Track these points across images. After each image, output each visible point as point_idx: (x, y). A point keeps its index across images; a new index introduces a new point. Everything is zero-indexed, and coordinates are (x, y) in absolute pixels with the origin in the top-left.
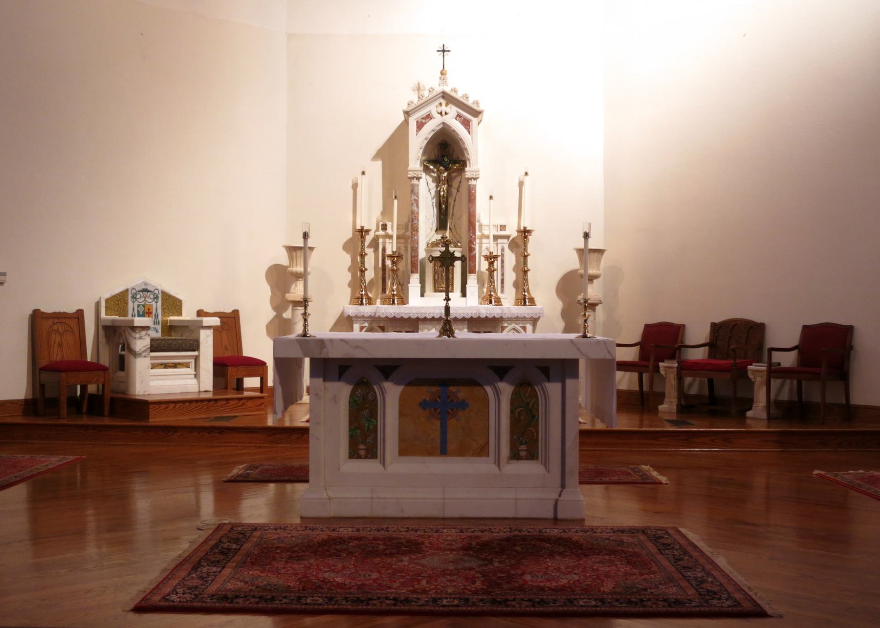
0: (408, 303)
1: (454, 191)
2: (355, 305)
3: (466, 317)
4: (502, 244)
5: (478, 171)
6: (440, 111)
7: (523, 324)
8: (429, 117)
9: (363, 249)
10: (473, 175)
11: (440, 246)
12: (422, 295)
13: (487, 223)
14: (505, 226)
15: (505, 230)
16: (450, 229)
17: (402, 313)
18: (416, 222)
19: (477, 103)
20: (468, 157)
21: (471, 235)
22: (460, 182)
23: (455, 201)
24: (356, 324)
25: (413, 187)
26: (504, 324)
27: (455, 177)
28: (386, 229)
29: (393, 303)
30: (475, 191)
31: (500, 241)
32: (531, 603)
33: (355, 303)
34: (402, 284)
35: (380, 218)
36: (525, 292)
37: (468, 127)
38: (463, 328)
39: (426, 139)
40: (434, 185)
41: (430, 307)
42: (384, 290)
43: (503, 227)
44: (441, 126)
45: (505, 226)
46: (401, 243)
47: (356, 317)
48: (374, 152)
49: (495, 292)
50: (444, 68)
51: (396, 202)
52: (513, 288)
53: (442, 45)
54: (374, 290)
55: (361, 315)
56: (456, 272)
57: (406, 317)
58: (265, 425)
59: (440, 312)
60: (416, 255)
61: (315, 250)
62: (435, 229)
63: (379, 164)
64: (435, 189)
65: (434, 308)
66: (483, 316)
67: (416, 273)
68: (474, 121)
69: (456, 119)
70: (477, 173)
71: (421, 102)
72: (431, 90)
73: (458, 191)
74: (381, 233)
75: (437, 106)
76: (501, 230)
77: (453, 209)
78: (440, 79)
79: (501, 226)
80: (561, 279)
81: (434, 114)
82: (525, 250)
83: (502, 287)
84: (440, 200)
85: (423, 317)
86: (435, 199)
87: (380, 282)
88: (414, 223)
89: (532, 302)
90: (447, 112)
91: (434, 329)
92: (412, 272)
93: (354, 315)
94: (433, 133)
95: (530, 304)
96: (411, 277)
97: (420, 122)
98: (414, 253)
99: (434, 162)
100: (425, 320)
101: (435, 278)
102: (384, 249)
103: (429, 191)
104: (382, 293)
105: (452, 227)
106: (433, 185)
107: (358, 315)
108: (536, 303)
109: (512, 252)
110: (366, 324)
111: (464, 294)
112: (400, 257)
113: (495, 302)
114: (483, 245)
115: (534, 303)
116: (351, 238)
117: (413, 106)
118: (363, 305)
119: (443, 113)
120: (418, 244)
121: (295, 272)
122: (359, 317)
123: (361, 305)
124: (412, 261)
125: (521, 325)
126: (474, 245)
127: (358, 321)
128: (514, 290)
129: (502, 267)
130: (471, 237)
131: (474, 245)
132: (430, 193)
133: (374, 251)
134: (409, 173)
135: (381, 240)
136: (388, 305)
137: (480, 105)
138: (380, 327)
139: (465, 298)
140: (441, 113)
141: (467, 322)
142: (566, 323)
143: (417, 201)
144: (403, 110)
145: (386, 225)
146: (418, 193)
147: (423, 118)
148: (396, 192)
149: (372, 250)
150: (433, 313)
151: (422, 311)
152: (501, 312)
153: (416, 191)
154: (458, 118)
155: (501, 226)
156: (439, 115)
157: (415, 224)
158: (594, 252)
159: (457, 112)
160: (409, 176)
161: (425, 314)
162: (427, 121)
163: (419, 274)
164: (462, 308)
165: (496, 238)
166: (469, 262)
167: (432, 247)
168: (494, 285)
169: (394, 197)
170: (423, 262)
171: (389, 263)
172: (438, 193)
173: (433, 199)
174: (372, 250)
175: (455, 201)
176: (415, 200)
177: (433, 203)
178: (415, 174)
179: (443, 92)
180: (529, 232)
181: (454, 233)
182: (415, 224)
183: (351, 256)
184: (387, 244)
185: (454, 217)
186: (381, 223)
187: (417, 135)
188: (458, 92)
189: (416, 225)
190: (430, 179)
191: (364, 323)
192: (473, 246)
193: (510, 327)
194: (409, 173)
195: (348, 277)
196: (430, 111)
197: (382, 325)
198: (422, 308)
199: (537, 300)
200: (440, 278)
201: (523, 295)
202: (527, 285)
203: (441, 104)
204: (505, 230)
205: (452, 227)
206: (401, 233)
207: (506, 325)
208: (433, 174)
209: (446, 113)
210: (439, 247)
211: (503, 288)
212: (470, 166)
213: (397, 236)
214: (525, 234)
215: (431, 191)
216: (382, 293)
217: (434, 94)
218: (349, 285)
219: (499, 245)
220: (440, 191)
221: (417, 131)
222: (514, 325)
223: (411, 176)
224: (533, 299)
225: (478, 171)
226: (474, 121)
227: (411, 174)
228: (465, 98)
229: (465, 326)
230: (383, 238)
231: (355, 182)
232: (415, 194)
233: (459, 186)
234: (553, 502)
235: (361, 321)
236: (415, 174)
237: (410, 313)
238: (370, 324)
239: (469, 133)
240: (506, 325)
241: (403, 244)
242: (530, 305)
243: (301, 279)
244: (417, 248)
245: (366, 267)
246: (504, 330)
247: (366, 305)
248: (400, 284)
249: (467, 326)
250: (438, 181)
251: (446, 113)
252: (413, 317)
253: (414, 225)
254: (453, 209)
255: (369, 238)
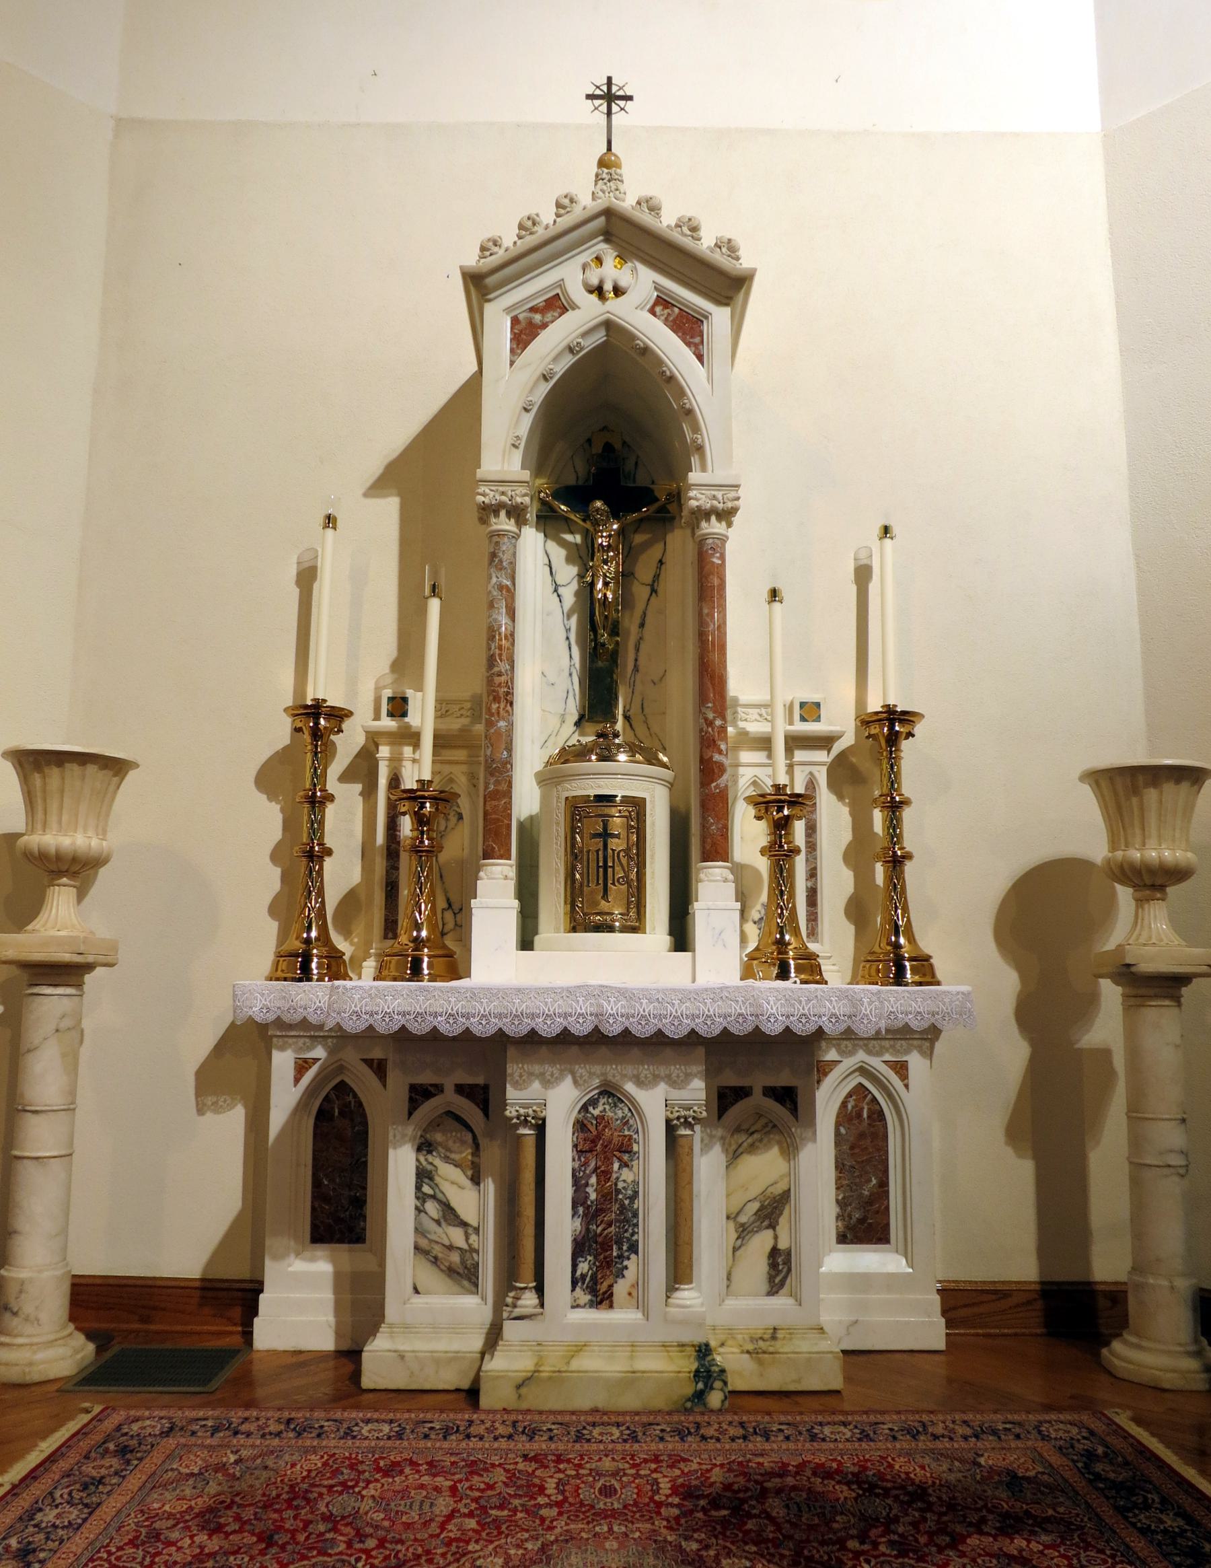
0: (468, 975)
1: (640, 592)
2: (277, 979)
3: (702, 1031)
4: (808, 769)
5: (738, 486)
6: (595, 282)
7: (897, 1052)
8: (556, 304)
9: (319, 776)
10: (714, 497)
11: (594, 757)
12: (526, 944)
13: (762, 696)
14: (818, 705)
15: (818, 719)
16: (627, 718)
17: (436, 1015)
18: (503, 666)
19: (731, 248)
20: (694, 441)
21: (711, 716)
22: (661, 562)
23: (642, 625)
24: (282, 1049)
25: (497, 543)
26: (827, 1052)
27: (646, 546)
28: (404, 714)
29: (416, 973)
30: (723, 557)
31: (800, 755)
32: (702, 1431)
33: (279, 974)
34: (456, 907)
35: (389, 679)
36: (897, 934)
37: (697, 340)
38: (688, 1077)
39: (545, 378)
40: (573, 570)
41: (553, 990)
42: (390, 928)
43: (811, 710)
44: (599, 337)
45: (818, 705)
46: (457, 763)
47: (279, 1023)
48: (374, 466)
49: (796, 932)
50: (609, 148)
51: (434, 605)
52: (848, 923)
53: (605, 81)
54: (359, 928)
55: (297, 1018)
56: (652, 856)
57: (448, 1029)
58: (508, 1060)
59: (594, 1010)
60: (504, 787)
61: (132, 775)
62: (576, 717)
63: (390, 506)
64: (574, 586)
65: (570, 992)
66: (773, 1028)
67: (501, 857)
68: (719, 318)
69: (652, 311)
70: (732, 495)
71: (530, 241)
72: (566, 202)
73: (654, 591)
74: (388, 723)
75: (584, 267)
76: (803, 719)
77: (637, 650)
78: (598, 177)
79: (802, 705)
80: (1009, 891)
81: (576, 292)
82: (893, 781)
83: (813, 918)
84: (592, 615)
85: (524, 1030)
86: (574, 619)
87: (379, 897)
88: (496, 669)
89: (926, 971)
90: (623, 283)
91: (569, 1080)
92: (487, 856)
93: (271, 1017)
94: (568, 361)
95: (917, 978)
96: (482, 874)
97: (523, 324)
98: (497, 783)
99: (578, 496)
100: (532, 1040)
101: (573, 880)
102: (395, 781)
103: (556, 590)
104: (386, 937)
105: (634, 711)
106: (568, 573)
107: (286, 1018)
108: (939, 975)
109: (841, 797)
110: (319, 1052)
111: (681, 938)
112: (444, 799)
113: (799, 970)
114: (742, 770)
115: (933, 975)
116: (285, 749)
117: (500, 255)
118: (309, 979)
119: (608, 287)
120: (509, 749)
121: (53, 851)
122: (291, 1027)
123: (300, 980)
124: (486, 814)
125: (887, 1057)
126: (720, 752)
127: (291, 1041)
128: (850, 929)
129: (812, 846)
130: (710, 723)
131: (720, 752)
132: (559, 596)
133: (361, 794)
134: (481, 490)
135: (384, 751)
136: (395, 979)
137: (741, 253)
138: (369, 1062)
139: (688, 955)
140: (599, 291)
141: (701, 1051)
142: (1033, 1043)
143: (509, 593)
144: (461, 268)
145: (405, 700)
146: (513, 564)
147: (533, 310)
148: (435, 573)
149: (358, 787)
150: (566, 1016)
151: (520, 1005)
152: (848, 1010)
153: (506, 558)
154: (658, 309)
155: (802, 705)
156: (594, 298)
157: (500, 674)
158: (1178, 781)
159: (657, 287)
160: (480, 499)
161: (533, 1016)
162: (549, 317)
163: (513, 861)
164: (686, 995)
165: (795, 742)
166: (704, 819)
167: (566, 762)
168: (794, 907)
169: (427, 591)
170: (529, 831)
171: (406, 826)
172: (587, 590)
173: (569, 617)
174: (358, 787)
175: (642, 625)
176: (501, 587)
177: (568, 630)
178: (503, 493)
179: (609, 213)
180: (907, 717)
181: (641, 730)
182: (500, 674)
183: (282, 810)
184: (405, 763)
185: (639, 676)
186: (388, 693)
187: (512, 363)
188: (663, 212)
189: (503, 679)
190: (558, 554)
191: (310, 1049)
192: (717, 757)
193: (849, 1063)
194: (481, 489)
195: (270, 880)
196: (560, 284)
197: (377, 1054)
198: (519, 991)
199: (940, 966)
200: (593, 877)
201: (889, 943)
202: (906, 910)
203: (599, 260)
204: (818, 719)
205: (634, 711)
206: (455, 724)
207: (832, 1055)
208: (569, 537)
209: (618, 291)
210: (590, 760)
211: (815, 920)
212: (704, 469)
213: (436, 737)
214: (891, 728)
215: (561, 590)
216: (386, 937)
217: (577, 214)
218: (273, 910)
219: (797, 769)
220: (592, 585)
221: (512, 351)
222: (861, 1056)
223: (487, 501)
224: (927, 958)
225: (738, 486)
226: (719, 318)
227: (488, 495)
228: (685, 229)
229: (695, 1069)
230: (391, 744)
231: (311, 564)
232: (500, 568)
233: (657, 577)
234: (734, 1286)
235: (301, 1041)
236: (503, 493)
237: (467, 1016)
238: (331, 1052)
239: (700, 358)
240: (832, 1055)
241: (464, 768)
242: (920, 984)
243: (65, 880)
244: (507, 765)
245: (329, 842)
246: (826, 1074)
247: (320, 979)
248: (450, 905)
249: (702, 1068)
250: (584, 556)
251: (618, 291)
252: (481, 1029)
253: (497, 680)
254: (637, 650)
255: (348, 742)
